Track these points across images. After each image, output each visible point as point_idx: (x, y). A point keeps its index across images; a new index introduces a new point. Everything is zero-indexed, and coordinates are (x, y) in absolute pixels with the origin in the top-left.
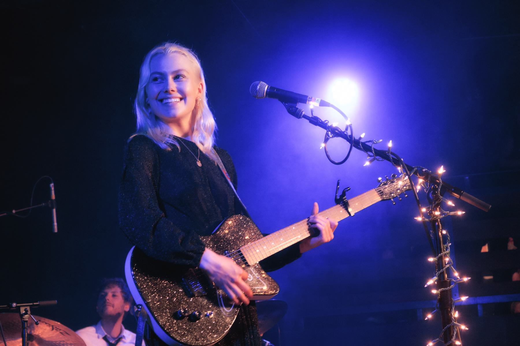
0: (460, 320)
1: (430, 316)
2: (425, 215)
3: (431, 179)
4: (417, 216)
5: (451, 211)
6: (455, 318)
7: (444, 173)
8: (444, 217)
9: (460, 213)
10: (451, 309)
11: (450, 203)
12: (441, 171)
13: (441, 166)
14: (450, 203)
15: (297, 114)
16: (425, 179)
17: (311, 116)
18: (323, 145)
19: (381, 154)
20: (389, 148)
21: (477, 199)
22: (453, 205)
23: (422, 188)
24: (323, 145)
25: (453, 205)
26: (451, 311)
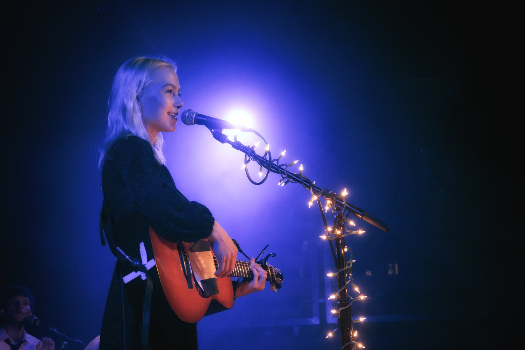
0: (358, 340)
1: (330, 335)
2: (329, 235)
3: (337, 200)
6: (353, 337)
7: (347, 195)
8: (346, 236)
9: (361, 232)
10: (350, 328)
11: (352, 223)
12: (345, 193)
13: (344, 189)
14: (352, 223)
15: (220, 138)
16: (332, 200)
17: (233, 141)
18: (244, 166)
20: (300, 172)
21: (370, 222)
22: (355, 225)
23: (330, 209)
25: (355, 225)
26: (350, 330)
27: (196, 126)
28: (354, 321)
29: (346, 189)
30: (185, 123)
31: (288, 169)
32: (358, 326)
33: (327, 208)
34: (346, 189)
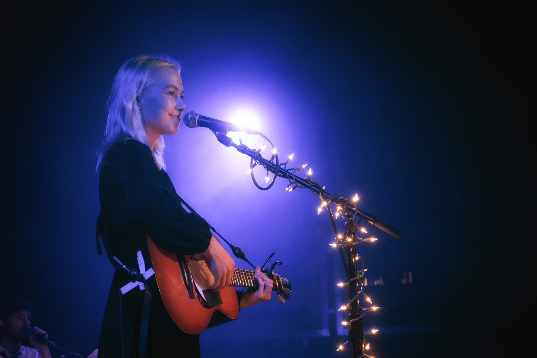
1: (341, 348)
2: (339, 242)
4: (331, 243)
5: (364, 238)
6: (365, 350)
7: (359, 201)
9: (373, 240)
10: (362, 341)
11: (363, 230)
14: (363, 230)
15: (225, 141)
16: (343, 206)
18: (250, 170)
19: (301, 182)
20: (309, 176)
23: (341, 216)
24: (250, 170)
26: (361, 343)
27: (199, 127)
28: (366, 333)
29: (357, 195)
30: (188, 125)
31: (296, 174)
32: (371, 339)
33: (337, 215)
34: (357, 195)
